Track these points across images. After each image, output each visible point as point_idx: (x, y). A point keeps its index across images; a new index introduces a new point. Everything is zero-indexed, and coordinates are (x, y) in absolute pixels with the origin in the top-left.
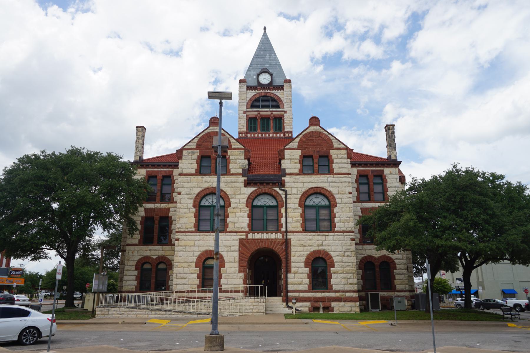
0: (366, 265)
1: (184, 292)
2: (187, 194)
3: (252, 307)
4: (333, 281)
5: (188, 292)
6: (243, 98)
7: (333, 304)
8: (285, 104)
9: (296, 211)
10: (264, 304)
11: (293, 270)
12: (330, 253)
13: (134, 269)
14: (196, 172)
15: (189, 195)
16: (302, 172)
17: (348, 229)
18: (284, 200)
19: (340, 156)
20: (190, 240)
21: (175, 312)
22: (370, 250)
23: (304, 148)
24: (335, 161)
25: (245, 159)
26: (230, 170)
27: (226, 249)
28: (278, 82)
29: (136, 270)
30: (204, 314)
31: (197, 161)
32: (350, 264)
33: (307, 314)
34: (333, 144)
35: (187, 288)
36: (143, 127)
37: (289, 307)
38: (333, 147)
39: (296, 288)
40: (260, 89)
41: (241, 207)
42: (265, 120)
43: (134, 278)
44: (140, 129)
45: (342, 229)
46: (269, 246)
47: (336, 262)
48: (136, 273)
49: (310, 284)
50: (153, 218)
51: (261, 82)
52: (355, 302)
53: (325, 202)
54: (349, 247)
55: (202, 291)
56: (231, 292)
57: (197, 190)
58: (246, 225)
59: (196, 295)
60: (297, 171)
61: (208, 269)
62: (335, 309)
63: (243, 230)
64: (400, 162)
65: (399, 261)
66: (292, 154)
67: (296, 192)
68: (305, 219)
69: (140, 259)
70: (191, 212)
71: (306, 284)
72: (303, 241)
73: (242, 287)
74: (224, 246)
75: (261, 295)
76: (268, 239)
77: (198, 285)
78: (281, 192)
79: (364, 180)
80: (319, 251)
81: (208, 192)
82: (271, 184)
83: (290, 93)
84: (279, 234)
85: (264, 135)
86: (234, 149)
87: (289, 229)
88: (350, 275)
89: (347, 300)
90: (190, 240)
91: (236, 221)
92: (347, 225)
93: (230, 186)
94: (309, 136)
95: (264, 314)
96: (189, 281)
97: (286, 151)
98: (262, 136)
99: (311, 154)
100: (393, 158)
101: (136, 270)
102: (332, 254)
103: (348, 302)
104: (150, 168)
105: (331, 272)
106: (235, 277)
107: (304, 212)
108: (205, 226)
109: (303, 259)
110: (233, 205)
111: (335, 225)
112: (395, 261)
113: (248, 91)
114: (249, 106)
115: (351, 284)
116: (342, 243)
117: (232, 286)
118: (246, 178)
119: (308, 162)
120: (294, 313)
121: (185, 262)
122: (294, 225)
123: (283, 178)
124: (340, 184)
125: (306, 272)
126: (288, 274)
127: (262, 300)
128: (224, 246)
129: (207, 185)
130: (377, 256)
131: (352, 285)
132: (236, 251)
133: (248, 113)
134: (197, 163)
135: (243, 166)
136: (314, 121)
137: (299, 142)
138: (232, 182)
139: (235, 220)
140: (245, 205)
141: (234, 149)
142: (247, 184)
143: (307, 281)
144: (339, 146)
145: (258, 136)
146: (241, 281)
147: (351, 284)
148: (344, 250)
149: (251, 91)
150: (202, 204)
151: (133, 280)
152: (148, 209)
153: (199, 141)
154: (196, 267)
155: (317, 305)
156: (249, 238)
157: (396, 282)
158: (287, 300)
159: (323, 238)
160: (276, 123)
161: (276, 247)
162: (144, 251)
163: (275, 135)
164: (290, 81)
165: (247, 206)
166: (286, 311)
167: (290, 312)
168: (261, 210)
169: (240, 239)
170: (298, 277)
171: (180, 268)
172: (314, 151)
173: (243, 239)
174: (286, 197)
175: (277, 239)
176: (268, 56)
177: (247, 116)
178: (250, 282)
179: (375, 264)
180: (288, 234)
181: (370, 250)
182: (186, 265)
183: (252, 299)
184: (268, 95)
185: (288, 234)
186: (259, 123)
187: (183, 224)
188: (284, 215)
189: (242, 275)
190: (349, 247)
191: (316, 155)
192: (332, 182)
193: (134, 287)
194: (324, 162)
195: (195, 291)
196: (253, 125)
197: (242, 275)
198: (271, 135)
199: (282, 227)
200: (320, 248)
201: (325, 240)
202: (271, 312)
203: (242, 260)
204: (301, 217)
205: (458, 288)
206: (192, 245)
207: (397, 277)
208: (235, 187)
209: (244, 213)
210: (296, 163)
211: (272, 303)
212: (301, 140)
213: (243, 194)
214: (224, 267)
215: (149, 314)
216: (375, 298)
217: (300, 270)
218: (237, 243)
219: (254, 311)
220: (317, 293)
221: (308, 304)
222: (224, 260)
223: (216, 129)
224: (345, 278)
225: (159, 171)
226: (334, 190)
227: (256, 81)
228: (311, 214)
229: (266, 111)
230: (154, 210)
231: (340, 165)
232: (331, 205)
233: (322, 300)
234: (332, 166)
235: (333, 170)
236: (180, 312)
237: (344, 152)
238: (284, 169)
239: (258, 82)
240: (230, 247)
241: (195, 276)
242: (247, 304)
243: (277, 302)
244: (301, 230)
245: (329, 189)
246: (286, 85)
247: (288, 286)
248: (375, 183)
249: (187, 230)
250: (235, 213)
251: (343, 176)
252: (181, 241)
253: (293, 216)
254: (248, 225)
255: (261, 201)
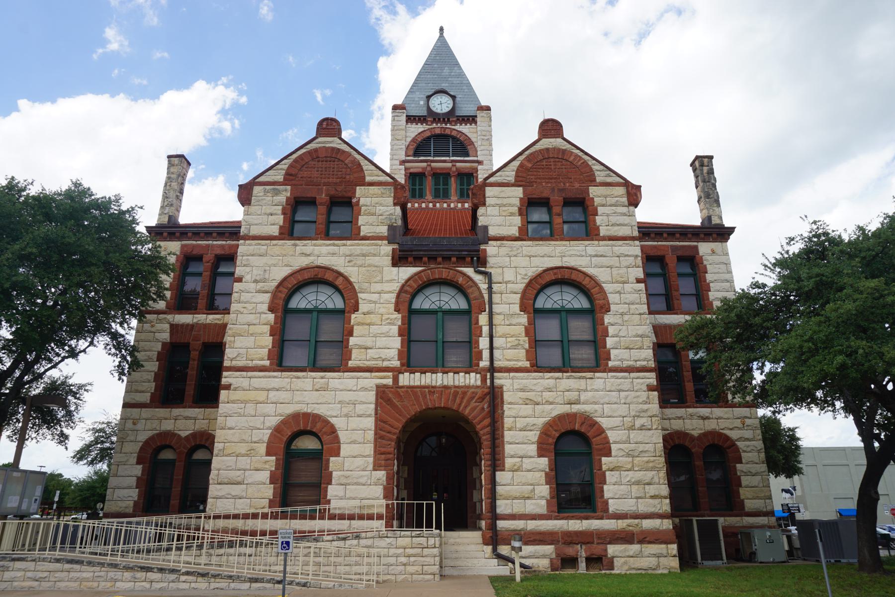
0: (677, 450)
1: (236, 517)
2: (256, 281)
3: (403, 560)
4: (609, 491)
5: (246, 516)
6: (399, 137)
7: (612, 550)
8: (478, 149)
9: (514, 321)
10: (436, 551)
11: (509, 462)
12: (598, 420)
13: (135, 460)
14: (280, 233)
15: (261, 284)
16: (523, 235)
17: (639, 364)
18: (486, 296)
19: (610, 200)
20: (257, 389)
21: (188, 573)
22: (679, 418)
23: (530, 184)
24: (600, 210)
25: (395, 204)
26: (359, 228)
27: (345, 410)
28: (466, 109)
29: (138, 463)
30: (269, 581)
31: (284, 209)
32: (650, 447)
33: (550, 578)
34: (594, 174)
35: (242, 507)
36: (181, 156)
37: (499, 557)
38: (595, 180)
39: (518, 507)
40: (432, 123)
41: (382, 311)
42: (441, 177)
43: (133, 481)
44: (176, 161)
45: (626, 364)
46: (450, 405)
47: (615, 442)
48: (138, 470)
49: (552, 498)
50: (186, 347)
51: (434, 109)
52: (666, 542)
53: (582, 303)
54: (646, 407)
55: (284, 516)
56: (351, 517)
57: (280, 273)
58: (394, 353)
59: (259, 524)
60: (514, 231)
61: (301, 462)
62: (617, 562)
63: (386, 364)
64: (731, 230)
65: (748, 443)
66: (502, 195)
67: (512, 278)
68: (536, 343)
69: (151, 439)
70: (263, 321)
71: (542, 498)
72: (531, 390)
73: (380, 505)
74: (340, 402)
75: (429, 525)
76: (446, 387)
77: (270, 501)
78: (477, 278)
79: (656, 269)
80: (571, 417)
81: (307, 275)
82: (454, 259)
83: (488, 128)
84: (473, 375)
85: (438, 205)
86: (371, 184)
87: (497, 364)
88: (650, 474)
89: (646, 538)
90: (257, 389)
91: (369, 344)
92: (635, 354)
93: (359, 262)
94: (541, 157)
95: (437, 577)
96: (250, 490)
97: (488, 189)
98: (435, 206)
99: (545, 195)
100: (715, 221)
101: (138, 463)
102: (604, 422)
103: (650, 542)
104: (189, 239)
105: (604, 467)
106: (363, 480)
107: (532, 322)
108: (296, 355)
109: (534, 436)
110: (363, 307)
111: (609, 353)
112: (738, 443)
113: (409, 125)
114: (412, 152)
115: (652, 497)
116: (626, 397)
117: (357, 503)
118: (396, 246)
119: (539, 215)
120: (518, 579)
121: (243, 441)
122: (510, 353)
123: (482, 247)
124: (614, 261)
125: (542, 467)
126: (498, 473)
127: (431, 541)
128: (340, 402)
129: (304, 262)
130: (695, 433)
131: (657, 501)
132: (369, 416)
133: (408, 165)
134: (284, 213)
135: (390, 219)
136: (550, 128)
137: (518, 171)
138: (364, 255)
139: (369, 342)
140: (392, 306)
141: (371, 184)
142: (399, 260)
143: (544, 490)
144: (609, 180)
145: (427, 206)
146: (379, 491)
147: (652, 497)
148: (633, 413)
149: (414, 125)
150: (293, 304)
151: (130, 488)
152: (177, 325)
153: (291, 166)
154: (268, 454)
155: (570, 551)
156: (401, 384)
157: (743, 493)
158: (494, 539)
159: (582, 384)
160: (462, 184)
161: (466, 407)
162: (160, 420)
163: (460, 205)
164: (488, 109)
165: (397, 310)
166: (494, 568)
167: (504, 570)
168: (429, 321)
169: (378, 387)
170: (522, 481)
171: (229, 455)
172: (553, 190)
173: (386, 386)
174: (490, 288)
175: (469, 387)
176: (446, 71)
177: (406, 169)
178: (404, 494)
179: (693, 450)
180: (496, 374)
181: (679, 418)
182: (243, 448)
183: (406, 539)
184: (448, 132)
185: (496, 374)
186: (429, 183)
187: (243, 351)
188: (485, 330)
189: (381, 474)
190: (646, 407)
191: (556, 199)
192: (596, 256)
193: (132, 504)
194: (577, 214)
195: (265, 516)
196: (417, 187)
197: (381, 474)
198: (452, 205)
199: (481, 359)
200: (575, 408)
201: (586, 390)
202: (455, 572)
203: (382, 437)
204: (527, 334)
205: (786, 508)
206: (261, 399)
207: (745, 481)
208: (369, 266)
209: (390, 324)
210: (512, 214)
211: (455, 547)
212: (521, 165)
213: (388, 281)
214: (337, 454)
215: (116, 581)
216: (709, 531)
217: (527, 463)
218: (371, 396)
219: (410, 569)
220: (571, 522)
221: (549, 549)
222: (337, 437)
223: (547, 143)
224: (638, 483)
225: (208, 246)
226: (601, 275)
227: (425, 109)
228: (550, 329)
229: (443, 163)
230: (192, 327)
231: (613, 219)
232: (596, 306)
233: (584, 538)
234: (595, 221)
235: (598, 229)
236: (203, 575)
237: (621, 190)
238: (486, 228)
239: (429, 109)
240: (348, 404)
241: (265, 476)
242: (392, 551)
243: (468, 544)
244: (527, 364)
245: (591, 271)
246: (480, 114)
247: (498, 503)
248: (680, 275)
249: (250, 364)
250: (369, 325)
251: (620, 243)
252: (235, 389)
253: (507, 333)
254: (400, 353)
255: (429, 300)
